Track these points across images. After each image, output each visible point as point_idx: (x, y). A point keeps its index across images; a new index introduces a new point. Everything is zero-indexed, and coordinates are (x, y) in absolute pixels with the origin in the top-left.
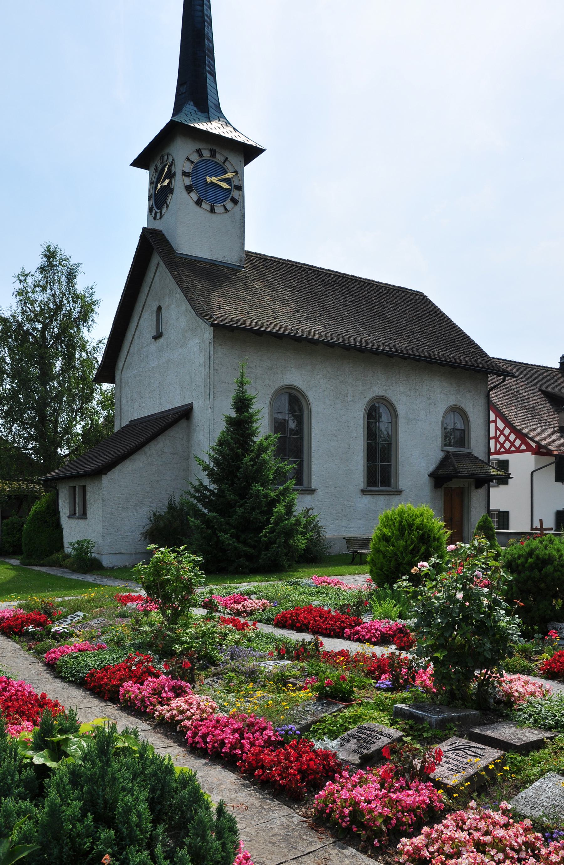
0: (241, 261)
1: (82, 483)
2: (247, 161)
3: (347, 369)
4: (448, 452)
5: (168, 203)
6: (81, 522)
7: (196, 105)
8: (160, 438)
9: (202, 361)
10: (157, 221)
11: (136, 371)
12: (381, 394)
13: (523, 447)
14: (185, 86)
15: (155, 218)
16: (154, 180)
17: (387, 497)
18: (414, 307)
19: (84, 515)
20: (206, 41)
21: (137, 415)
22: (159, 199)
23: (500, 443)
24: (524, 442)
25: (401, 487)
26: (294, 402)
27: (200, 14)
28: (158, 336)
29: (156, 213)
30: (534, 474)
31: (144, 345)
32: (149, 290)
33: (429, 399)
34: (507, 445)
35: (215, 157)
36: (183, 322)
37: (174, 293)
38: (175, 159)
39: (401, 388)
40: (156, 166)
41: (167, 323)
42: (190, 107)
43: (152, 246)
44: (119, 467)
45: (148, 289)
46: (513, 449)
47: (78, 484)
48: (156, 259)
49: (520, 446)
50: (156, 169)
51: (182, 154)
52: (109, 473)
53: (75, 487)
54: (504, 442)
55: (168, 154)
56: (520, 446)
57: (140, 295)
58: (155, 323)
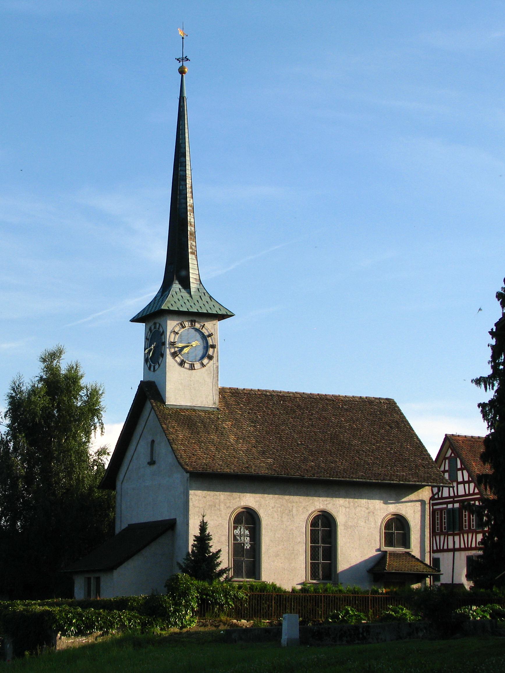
0: (215, 403)
1: (97, 575)
5: (160, 362)
7: (181, 283)
12: (322, 507)
15: (150, 369)
22: (154, 358)
26: (249, 519)
28: (152, 463)
29: (150, 365)
33: (367, 509)
42: (176, 286)
44: (125, 564)
47: (92, 576)
52: (118, 569)
53: (89, 579)
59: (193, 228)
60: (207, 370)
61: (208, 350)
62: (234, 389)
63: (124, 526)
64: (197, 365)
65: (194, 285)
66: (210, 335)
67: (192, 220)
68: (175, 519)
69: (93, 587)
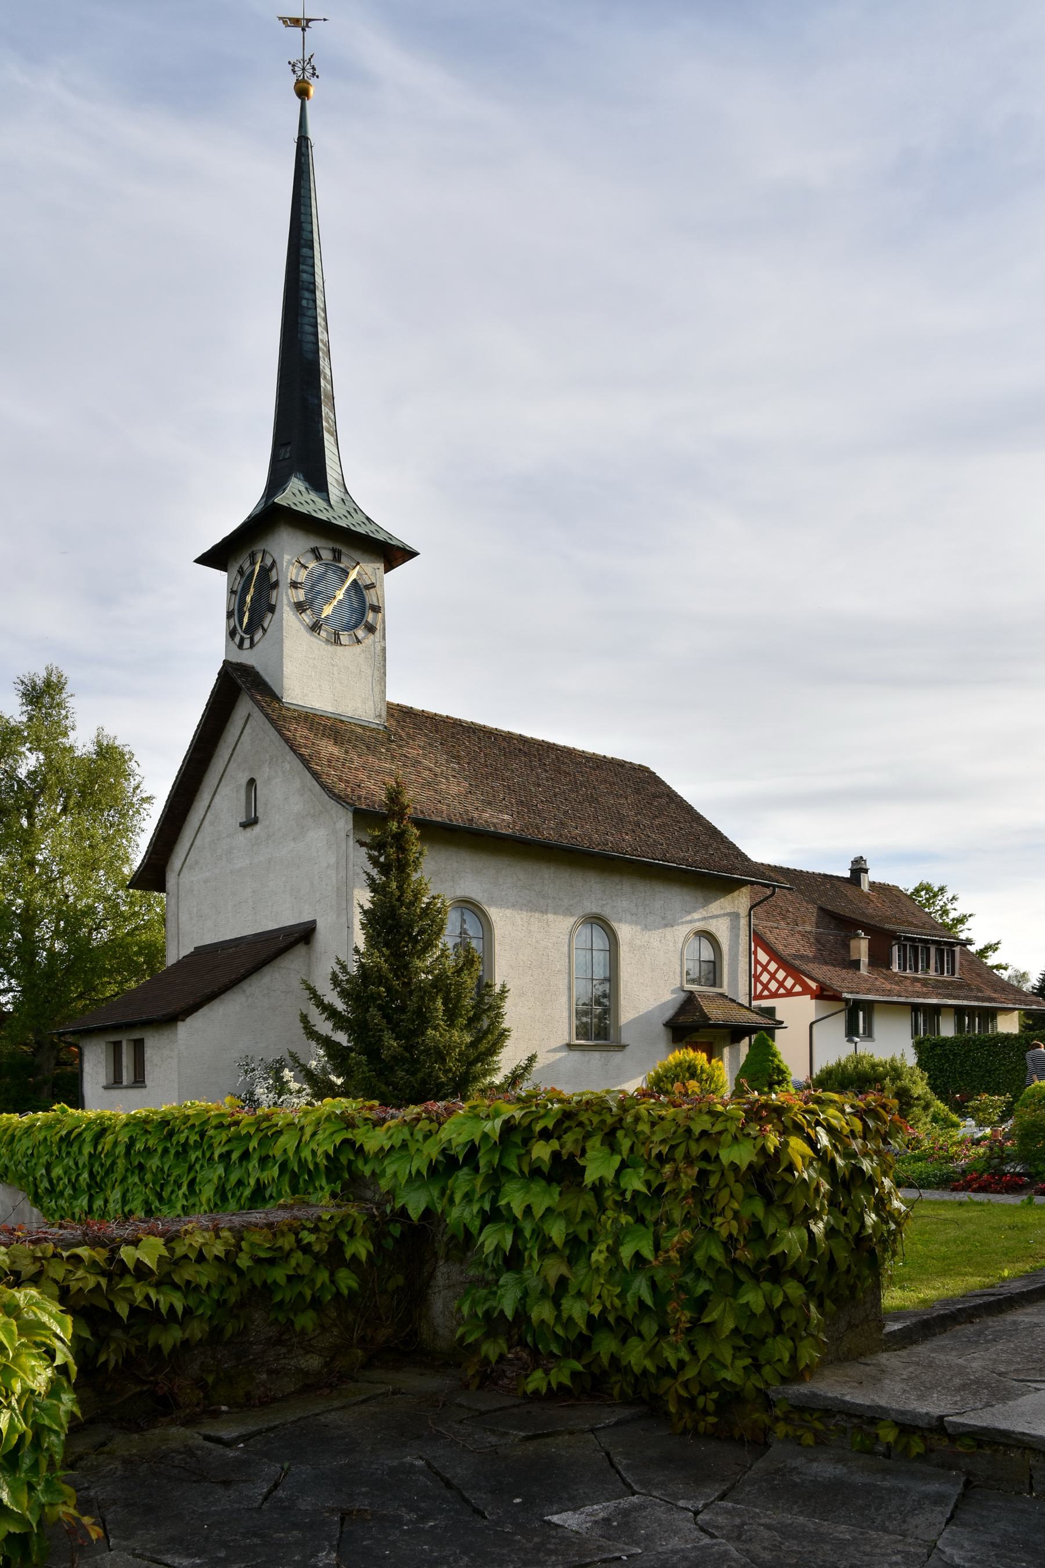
1: (136, 1035)
2: (390, 565)
3: (546, 876)
4: (691, 992)
5: (266, 625)
6: (134, 1094)
8: (265, 969)
9: (333, 860)
10: (245, 652)
11: (208, 874)
12: (594, 910)
13: (798, 989)
14: (289, 449)
15: (240, 646)
16: (238, 587)
17: (604, 1054)
18: (639, 787)
19: (139, 1080)
20: (322, 381)
21: (209, 939)
22: (251, 612)
23: (761, 983)
24: (798, 981)
25: (624, 1041)
27: (311, 338)
28: (250, 823)
29: (242, 640)
30: (815, 1026)
31: (224, 836)
32: (232, 754)
33: (663, 919)
34: (773, 986)
35: (340, 561)
36: (296, 805)
37: (280, 761)
38: (277, 561)
39: (623, 903)
40: (241, 567)
41: (266, 805)
43: (238, 689)
45: (230, 751)
46: (782, 991)
48: (245, 707)
49: (793, 986)
50: (241, 572)
51: (291, 557)
52: (188, 1020)
53: (117, 1046)
54: (769, 982)
55: (264, 552)
56: (793, 986)
57: (214, 760)
58: (243, 803)
59: (329, 387)
60: (363, 651)
61: (363, 614)
62: (406, 707)
63: (187, 950)
64: (344, 638)
65: (334, 491)
66: (372, 586)
67: (328, 371)
68: (314, 922)
69: (479, 913)
